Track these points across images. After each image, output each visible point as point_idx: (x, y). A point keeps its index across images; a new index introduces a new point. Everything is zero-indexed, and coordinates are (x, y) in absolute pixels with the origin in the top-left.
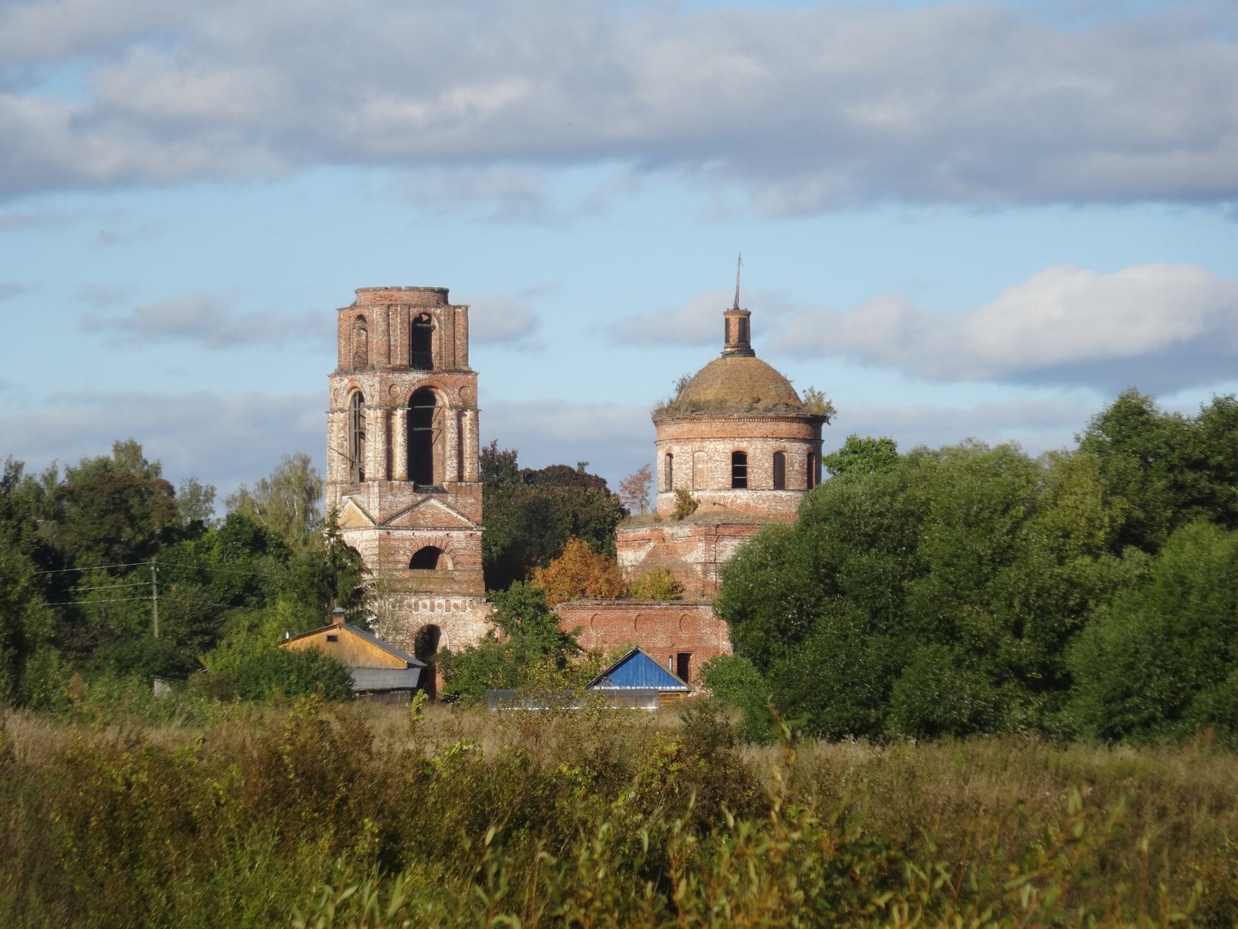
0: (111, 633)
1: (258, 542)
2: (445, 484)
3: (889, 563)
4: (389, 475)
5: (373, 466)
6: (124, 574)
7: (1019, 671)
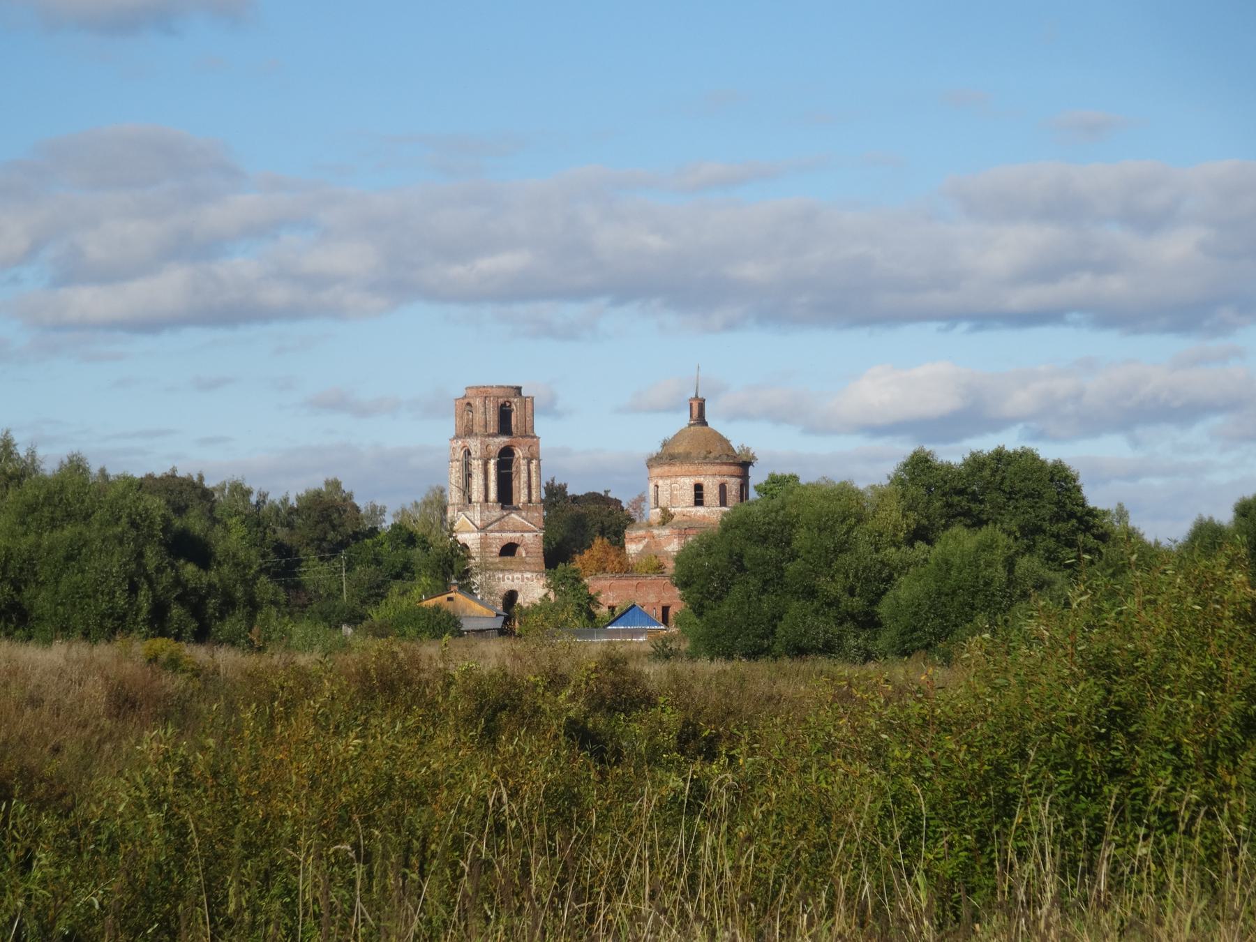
0: (321, 596)
1: (412, 540)
2: (520, 505)
3: (772, 552)
4: (486, 499)
5: (477, 494)
6: (328, 560)
7: (853, 617)
